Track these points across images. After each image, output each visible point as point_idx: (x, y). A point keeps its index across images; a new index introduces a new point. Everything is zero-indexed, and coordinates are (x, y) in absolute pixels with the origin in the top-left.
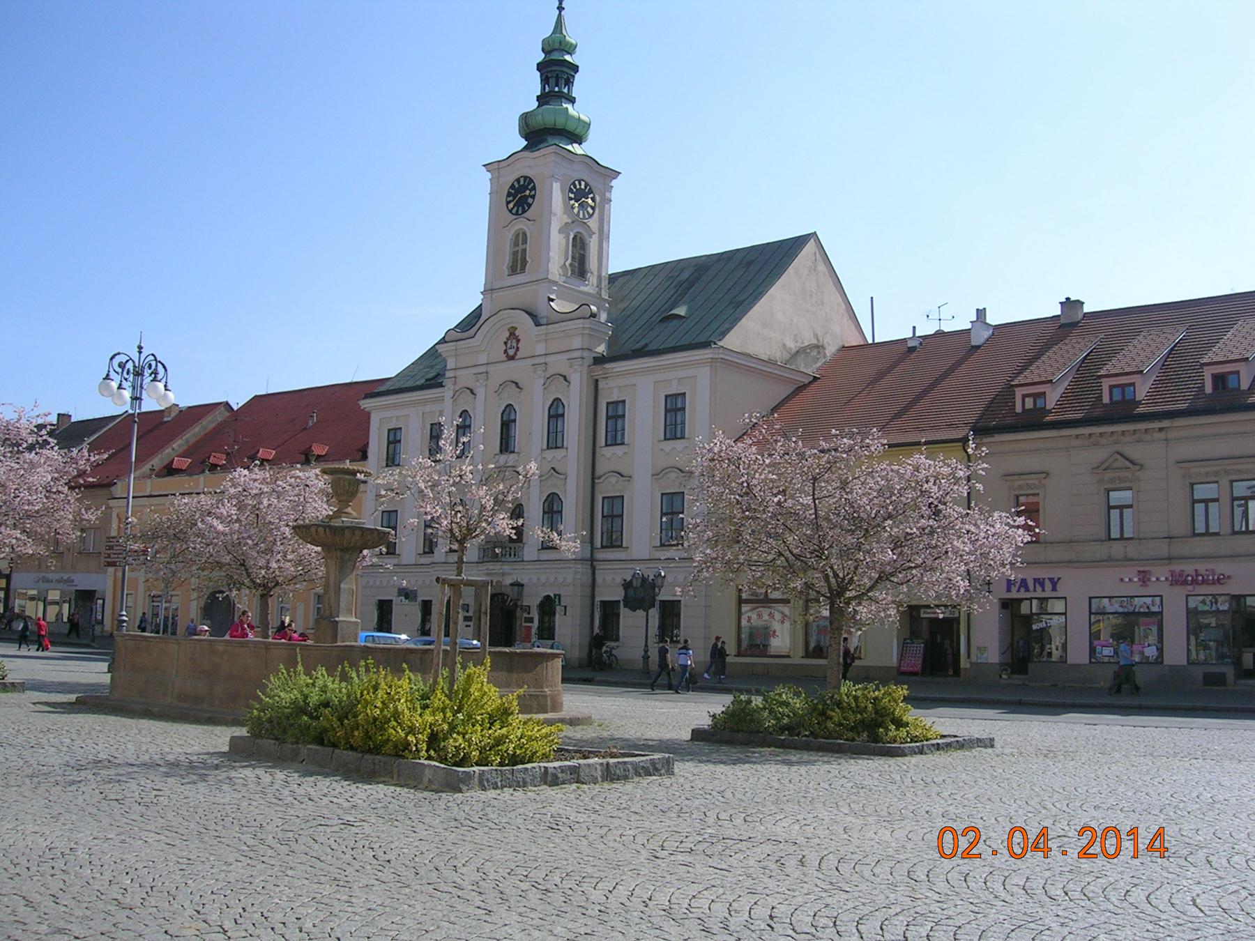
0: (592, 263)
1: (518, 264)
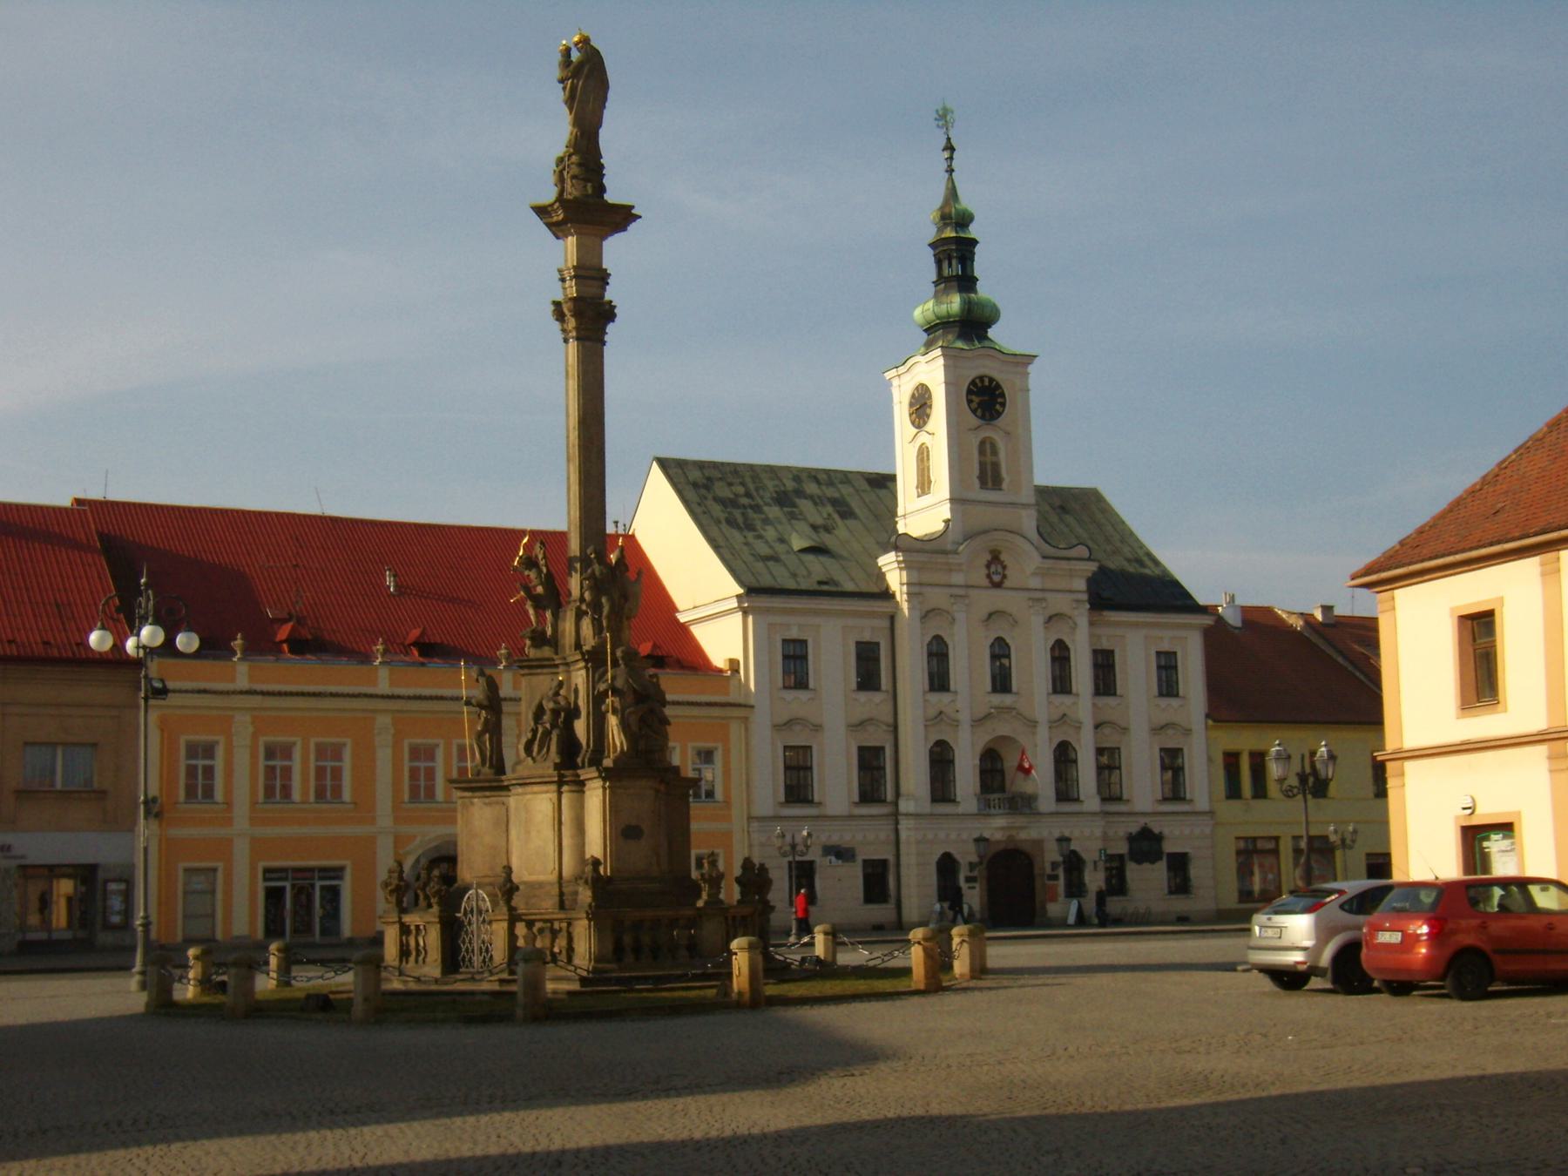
1: (990, 476)
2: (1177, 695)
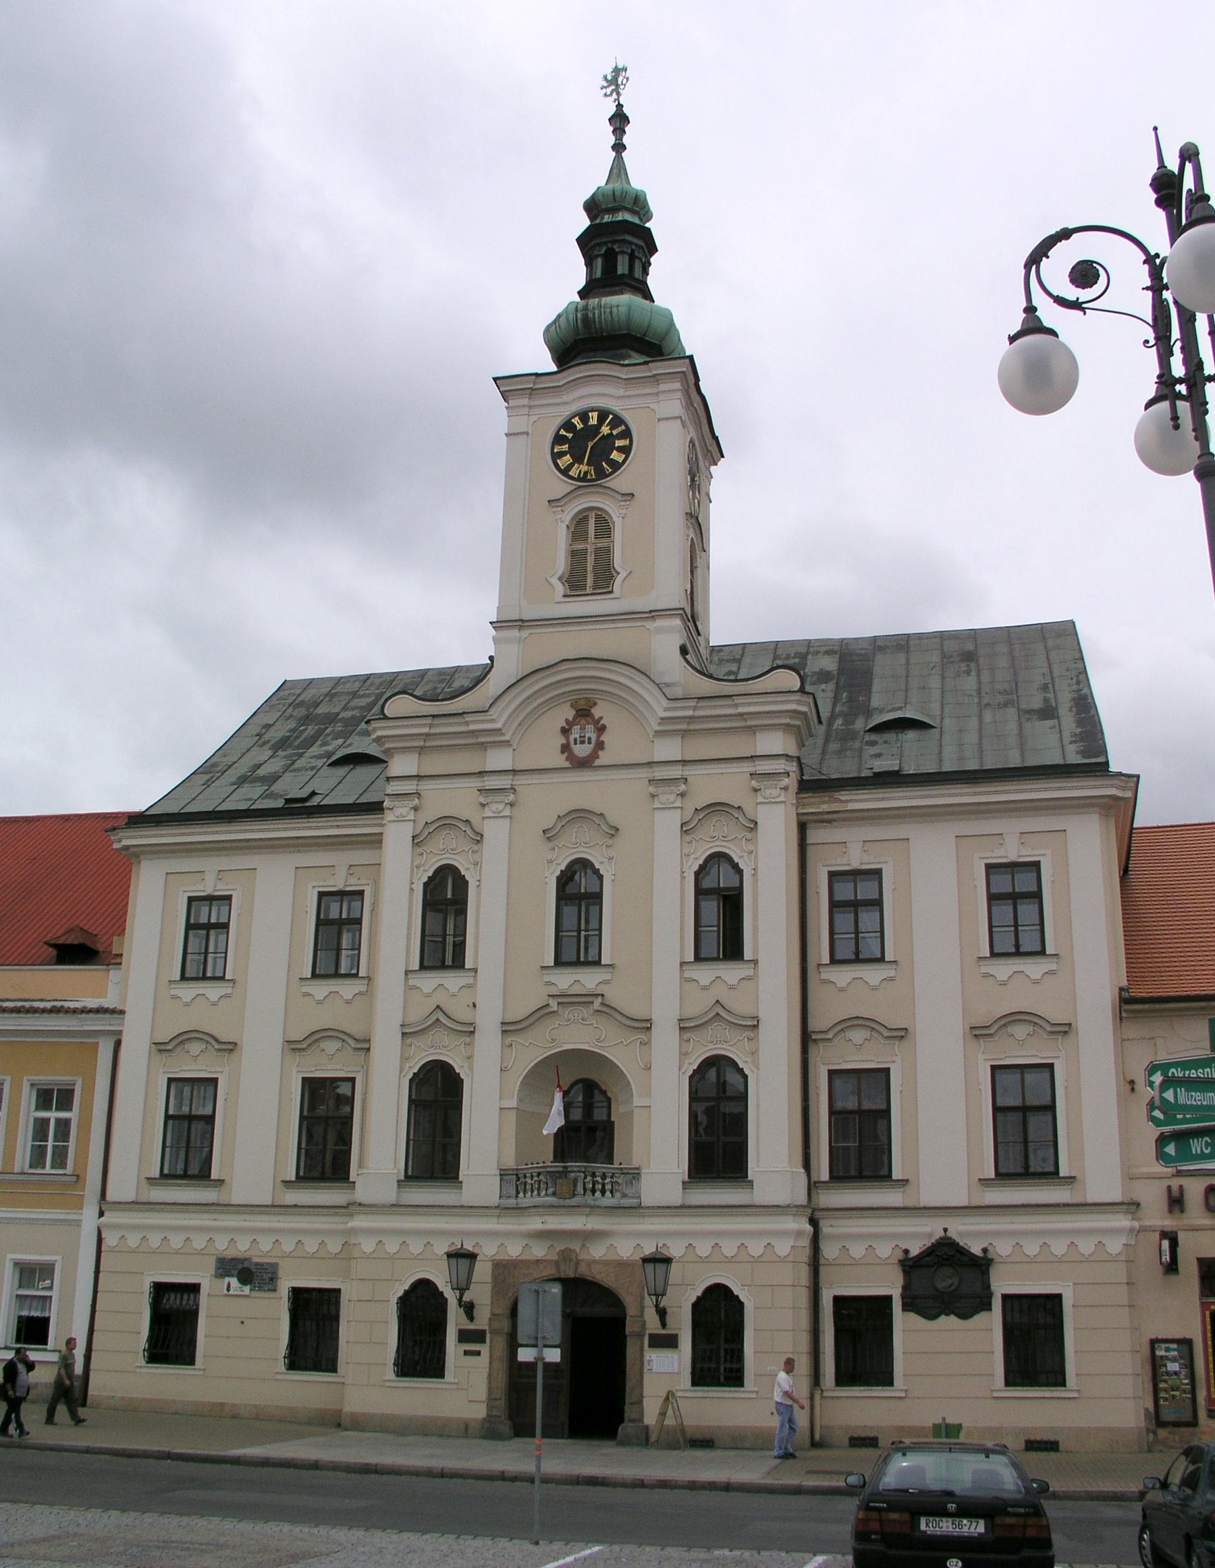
1: (590, 571)
2: (597, 963)
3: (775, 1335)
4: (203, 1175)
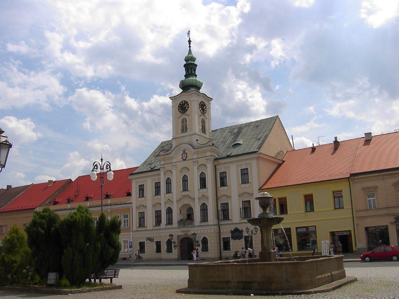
0: (207, 128)
1: (184, 129)
3: (213, 245)
4: (228, 219)
